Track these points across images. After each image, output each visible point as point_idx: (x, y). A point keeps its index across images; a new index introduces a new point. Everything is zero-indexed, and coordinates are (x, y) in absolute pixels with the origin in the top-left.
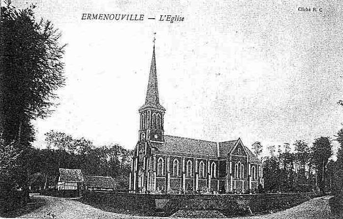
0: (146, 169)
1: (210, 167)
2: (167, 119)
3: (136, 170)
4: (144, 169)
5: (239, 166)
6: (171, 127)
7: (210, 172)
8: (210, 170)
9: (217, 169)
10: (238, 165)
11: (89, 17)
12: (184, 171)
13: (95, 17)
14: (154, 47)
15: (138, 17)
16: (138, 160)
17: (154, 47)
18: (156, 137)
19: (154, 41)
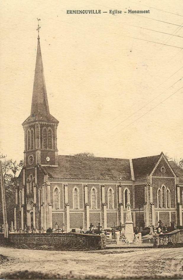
0: (37, 201)
1: (122, 195)
2: (60, 132)
3: (23, 203)
4: (35, 202)
5: (163, 190)
6: (67, 145)
7: (123, 201)
8: (122, 198)
9: (131, 196)
10: (161, 190)
11: (71, 13)
12: (104, 202)
13: (74, 12)
14: (39, 39)
15: (98, 12)
16: (25, 191)
17: (39, 39)
18: (48, 159)
19: (38, 29)
